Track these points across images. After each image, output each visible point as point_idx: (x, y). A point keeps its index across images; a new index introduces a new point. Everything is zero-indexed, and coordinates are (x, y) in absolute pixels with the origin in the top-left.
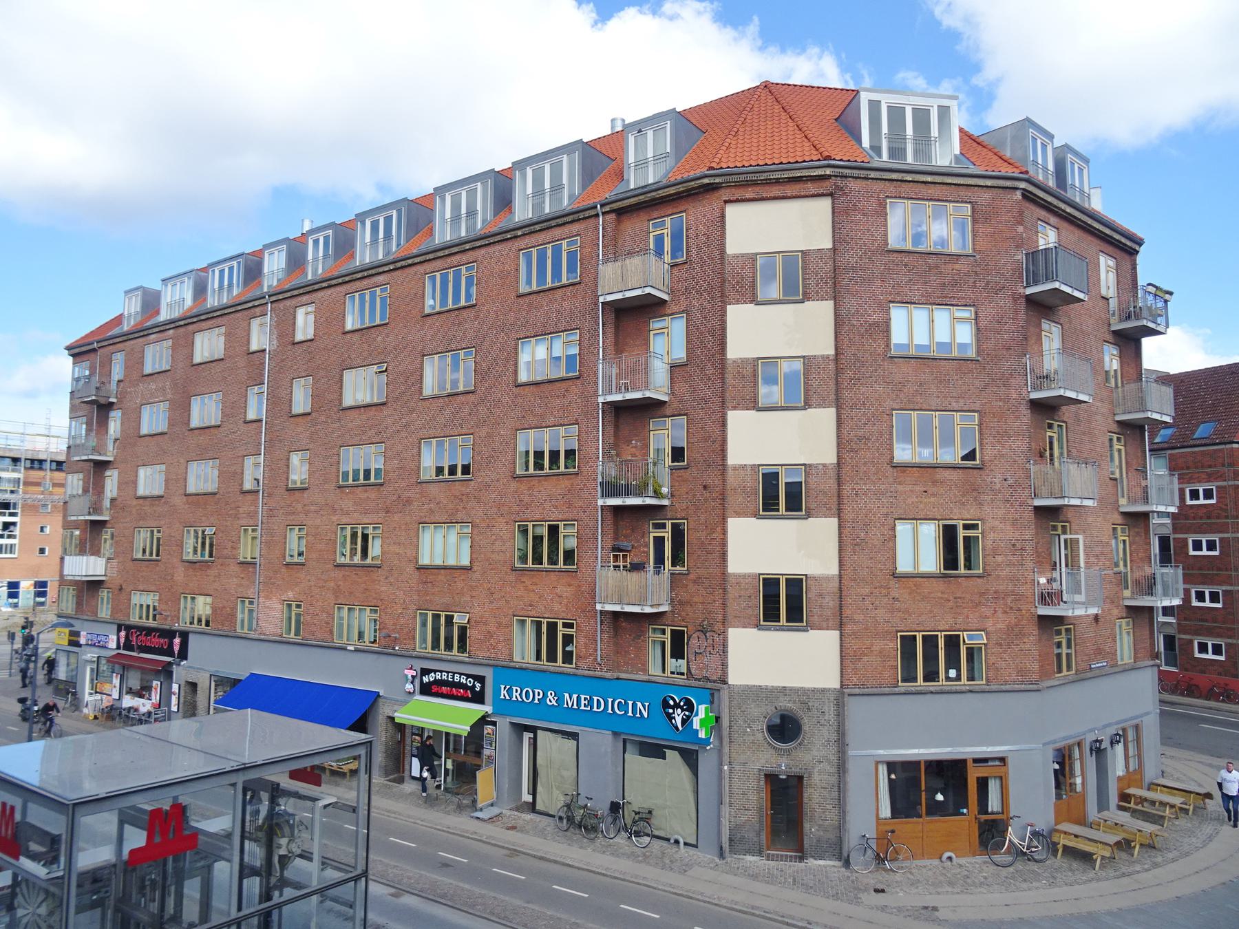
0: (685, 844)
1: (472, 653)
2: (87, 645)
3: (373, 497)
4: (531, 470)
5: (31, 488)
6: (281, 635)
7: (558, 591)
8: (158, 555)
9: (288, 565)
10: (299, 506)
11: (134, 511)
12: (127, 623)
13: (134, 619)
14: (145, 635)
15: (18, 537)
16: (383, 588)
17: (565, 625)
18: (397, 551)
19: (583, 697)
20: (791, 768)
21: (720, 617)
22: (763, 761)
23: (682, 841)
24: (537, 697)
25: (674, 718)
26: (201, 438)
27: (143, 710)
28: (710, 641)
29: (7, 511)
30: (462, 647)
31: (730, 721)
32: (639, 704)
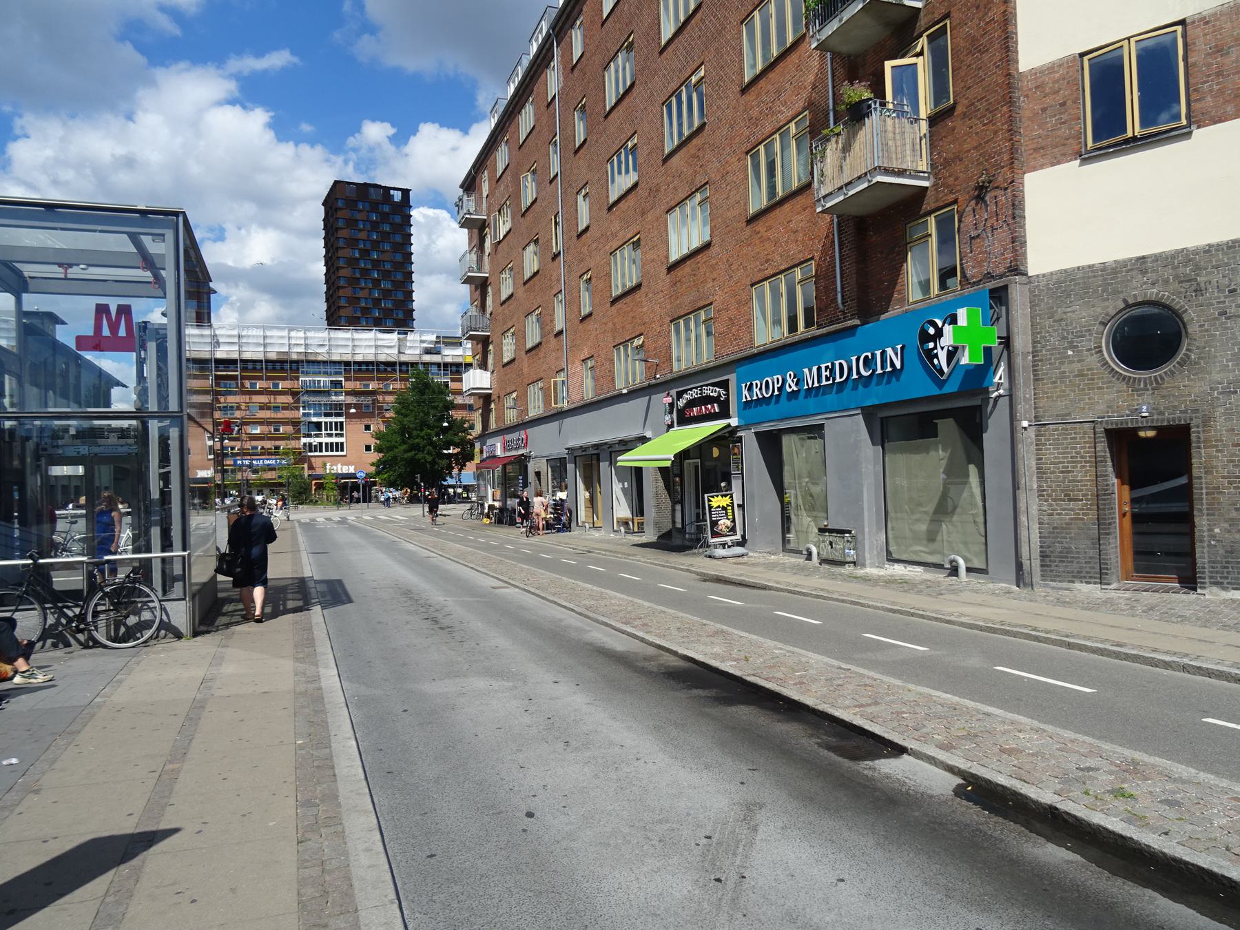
0: (969, 570)
7: (792, 225)
19: (823, 366)
20: (1161, 413)
21: (1006, 157)
22: (1101, 407)
23: (962, 564)
24: (776, 386)
25: (936, 356)
28: (991, 208)
31: (1034, 342)
32: (889, 351)
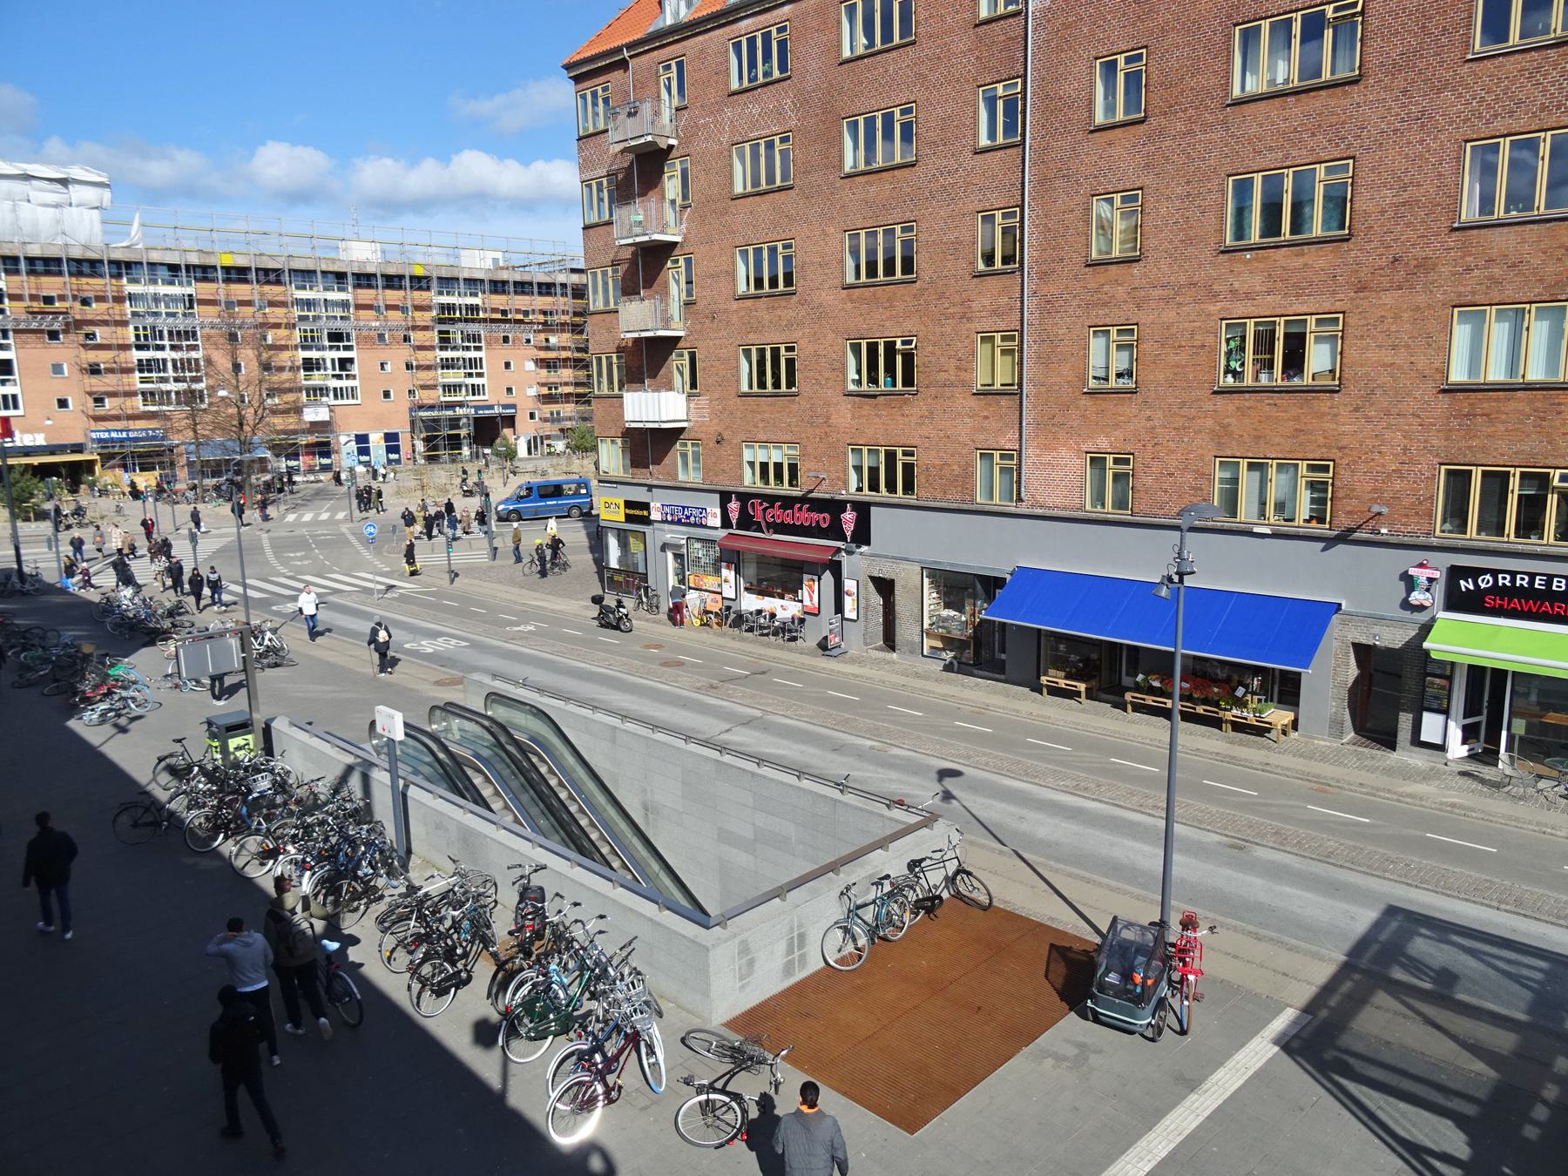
1: (1135, 510)
2: (663, 522)
3: (1322, 263)
4: (863, 278)
5: (362, 312)
6: (1082, 508)
8: (790, 384)
9: (1092, 393)
10: (1120, 292)
11: (735, 319)
12: (742, 490)
13: (750, 481)
14: (780, 507)
15: (357, 377)
16: (1346, 428)
17: (905, 454)
18: (1388, 360)
26: (872, 190)
27: (782, 615)
29: (341, 344)
30: (909, 487)
